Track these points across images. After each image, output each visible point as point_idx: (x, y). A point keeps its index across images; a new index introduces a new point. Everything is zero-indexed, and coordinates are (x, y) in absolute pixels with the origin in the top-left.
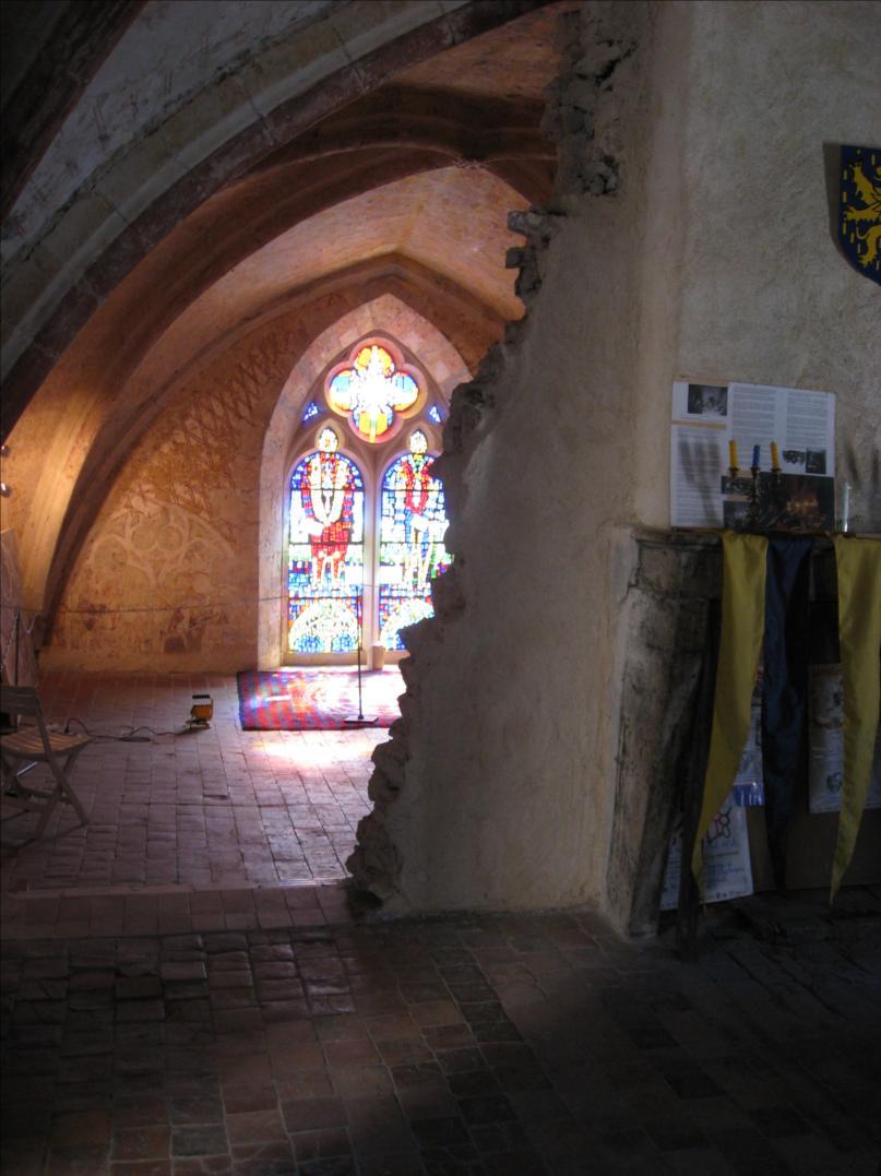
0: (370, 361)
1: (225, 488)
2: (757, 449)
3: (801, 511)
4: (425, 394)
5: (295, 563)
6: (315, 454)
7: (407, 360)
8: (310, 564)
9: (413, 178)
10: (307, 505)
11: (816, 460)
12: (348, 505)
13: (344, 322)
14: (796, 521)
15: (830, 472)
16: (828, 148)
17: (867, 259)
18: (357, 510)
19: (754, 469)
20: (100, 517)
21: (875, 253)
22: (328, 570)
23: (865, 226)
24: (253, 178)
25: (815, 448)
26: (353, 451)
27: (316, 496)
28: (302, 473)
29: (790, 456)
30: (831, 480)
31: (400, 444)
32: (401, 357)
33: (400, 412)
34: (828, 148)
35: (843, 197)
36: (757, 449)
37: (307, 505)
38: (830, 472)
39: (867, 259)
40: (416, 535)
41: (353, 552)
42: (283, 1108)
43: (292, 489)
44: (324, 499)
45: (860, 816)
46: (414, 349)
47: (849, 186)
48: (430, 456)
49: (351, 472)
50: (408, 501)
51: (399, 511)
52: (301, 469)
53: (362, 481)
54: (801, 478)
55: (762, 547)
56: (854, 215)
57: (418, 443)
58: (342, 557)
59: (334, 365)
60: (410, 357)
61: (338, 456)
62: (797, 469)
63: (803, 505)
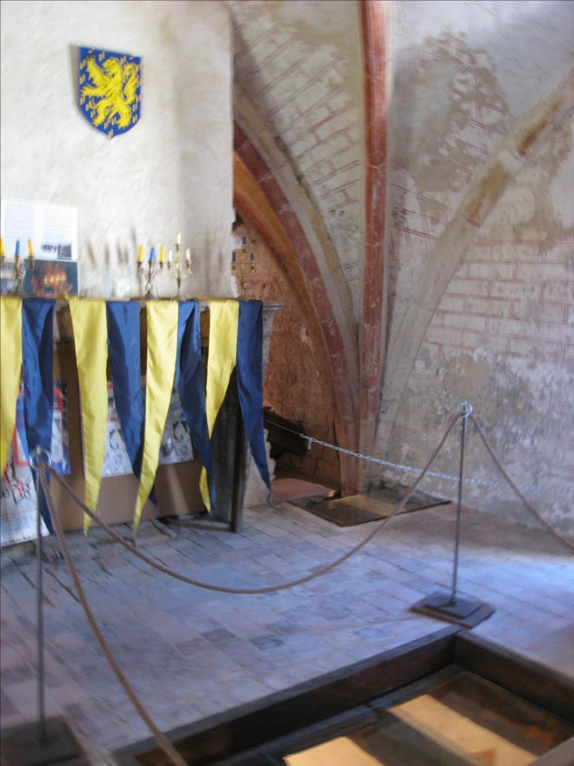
1: (253, 292)
2: (18, 244)
3: (54, 283)
11: (67, 251)
14: (50, 289)
15: (74, 258)
16: (72, 48)
17: (99, 121)
19: (17, 256)
23: (97, 100)
24: (407, 515)
25: (64, 242)
29: (47, 247)
30: (75, 265)
34: (72, 48)
35: (83, 80)
36: (18, 244)
38: (74, 258)
39: (99, 121)
45: (100, 480)
47: (84, 72)
51: (515, 273)
54: (54, 263)
55: (18, 306)
56: (88, 91)
62: (52, 256)
63: (57, 279)
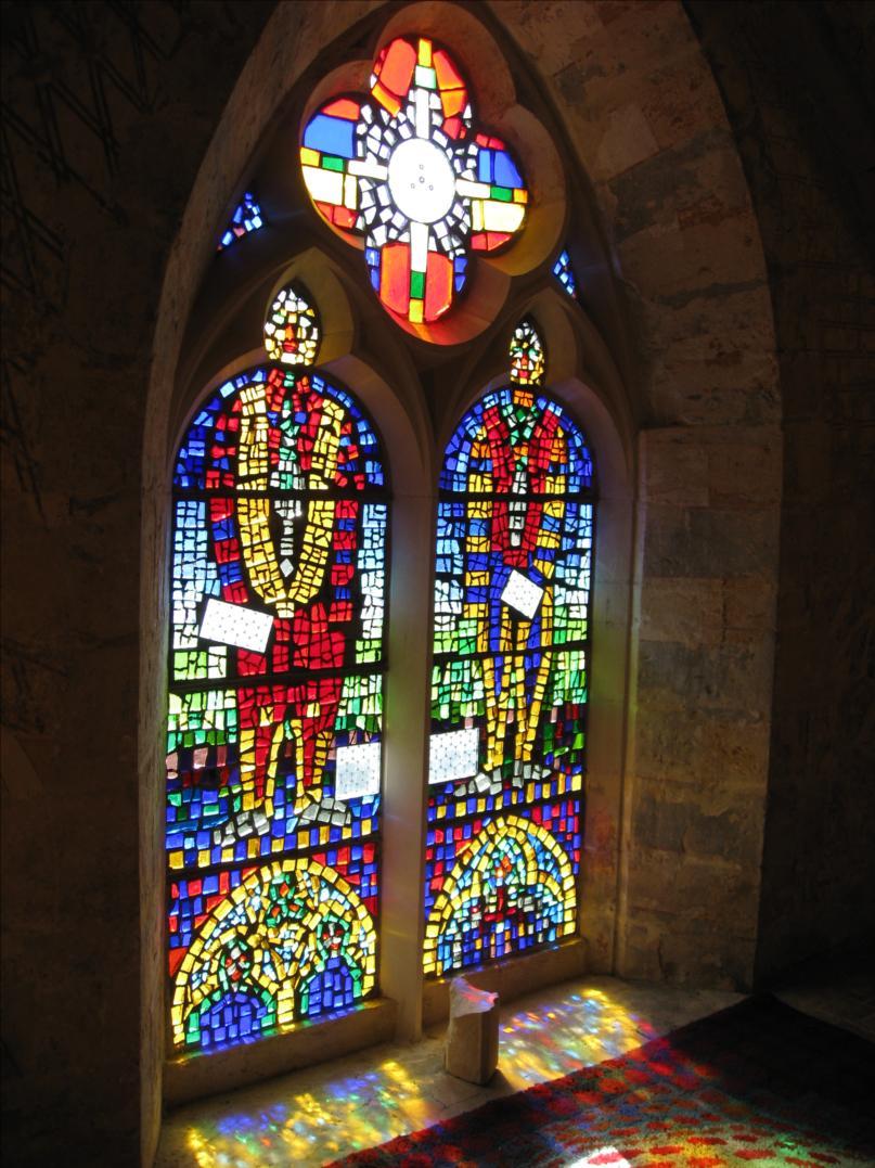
0: (421, 167)
4: (557, 211)
5: (185, 755)
6: (251, 372)
7: (523, 98)
8: (234, 753)
9: (499, 1061)
10: (225, 552)
12: (348, 535)
13: (360, 14)
18: (371, 557)
20: (250, 1111)
21: (718, 814)
22: (287, 765)
26: (306, 72)
27: (254, 521)
28: (208, 436)
31: (490, 357)
32: (504, 83)
33: (485, 254)
37: (225, 552)
40: (514, 630)
41: (361, 698)
42: (630, 869)
43: (179, 494)
44: (275, 524)
46: (547, 68)
48: (552, 397)
49: (354, 437)
50: (495, 529)
52: (204, 420)
53: (385, 471)
57: (528, 363)
58: (329, 713)
59: (320, 77)
60: (530, 90)
61: (318, 384)
